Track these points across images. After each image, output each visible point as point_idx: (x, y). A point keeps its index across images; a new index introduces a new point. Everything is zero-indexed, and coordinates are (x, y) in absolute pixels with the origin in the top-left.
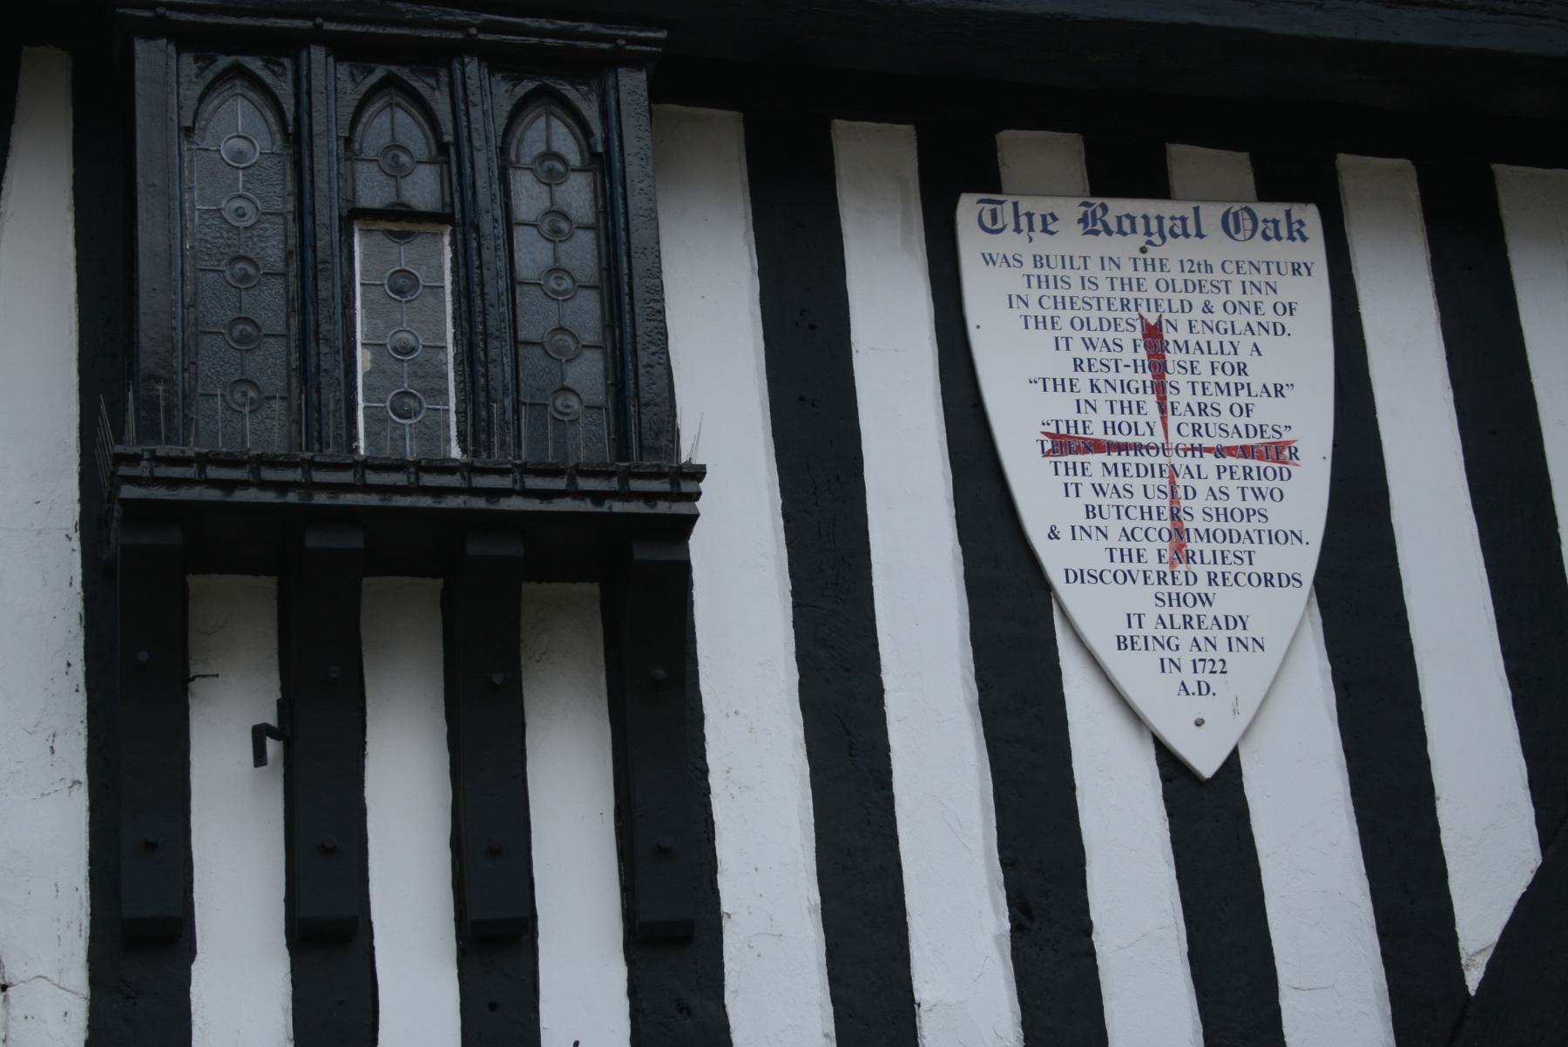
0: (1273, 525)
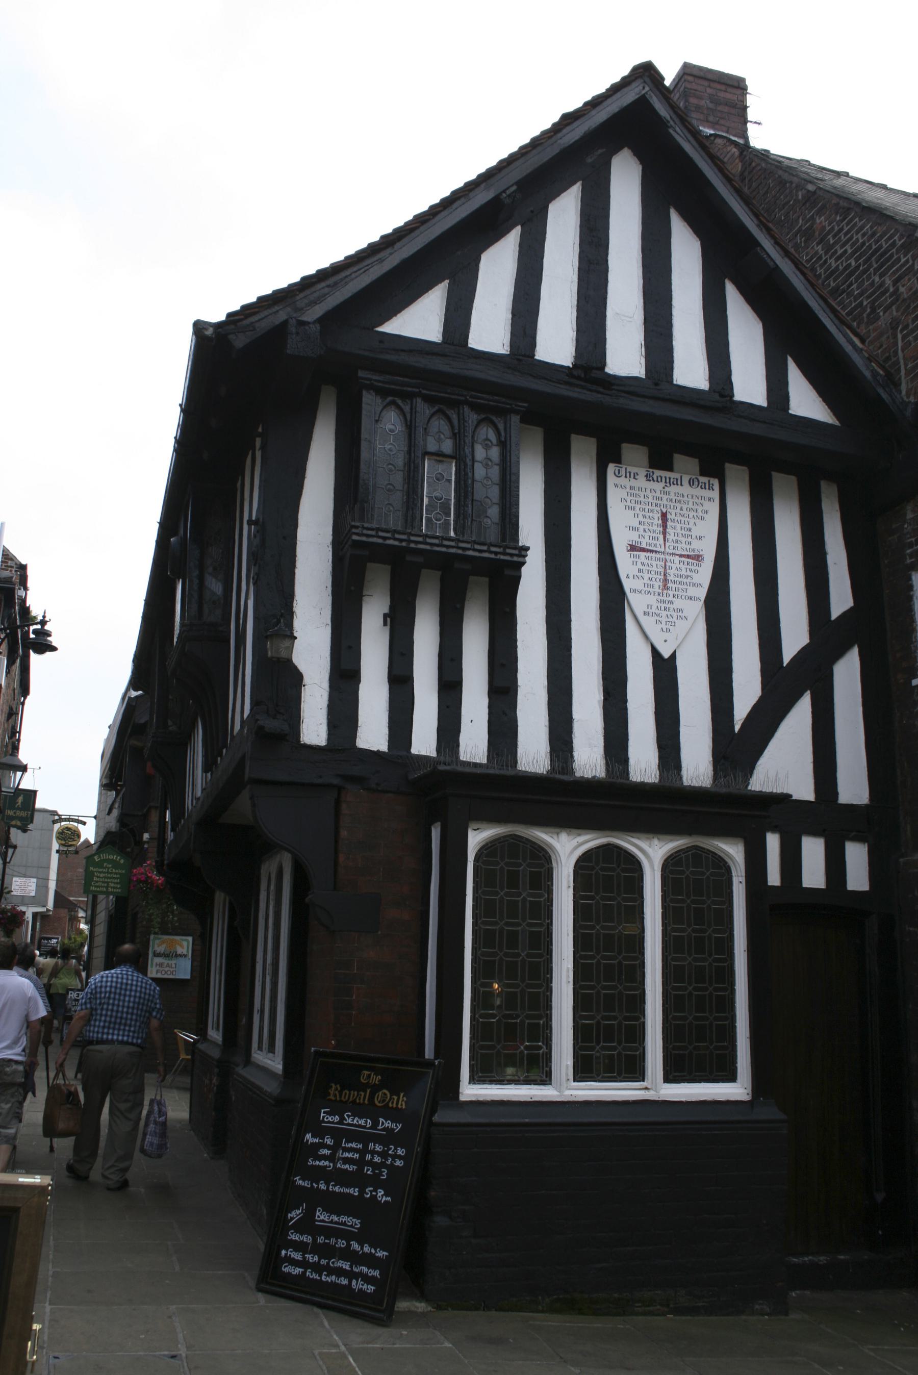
0: (694, 581)
